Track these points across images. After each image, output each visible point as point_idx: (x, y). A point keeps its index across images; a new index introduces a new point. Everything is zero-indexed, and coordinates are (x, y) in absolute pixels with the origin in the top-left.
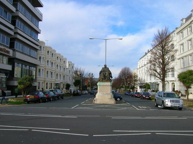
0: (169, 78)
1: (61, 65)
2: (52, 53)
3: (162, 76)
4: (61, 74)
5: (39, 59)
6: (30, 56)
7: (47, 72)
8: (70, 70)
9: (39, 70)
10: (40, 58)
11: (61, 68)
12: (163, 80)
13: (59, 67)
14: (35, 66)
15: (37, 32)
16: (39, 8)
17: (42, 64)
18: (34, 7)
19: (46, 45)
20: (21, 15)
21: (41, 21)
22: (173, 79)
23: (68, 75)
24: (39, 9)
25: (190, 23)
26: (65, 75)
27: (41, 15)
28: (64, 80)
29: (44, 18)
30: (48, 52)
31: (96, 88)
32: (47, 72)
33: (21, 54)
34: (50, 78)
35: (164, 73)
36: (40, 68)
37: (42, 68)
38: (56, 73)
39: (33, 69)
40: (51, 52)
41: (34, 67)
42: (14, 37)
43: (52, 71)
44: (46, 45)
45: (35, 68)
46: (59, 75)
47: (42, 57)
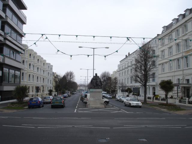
0: (151, 83)
1: (34, 64)
2: (34, 55)
3: (144, 81)
4: (35, 75)
5: (22, 63)
6: (15, 60)
7: (29, 75)
8: (48, 73)
9: (23, 73)
10: (23, 62)
11: (35, 67)
12: (145, 85)
13: (32, 66)
14: (19, 69)
15: (21, 36)
16: (23, 10)
17: (25, 67)
18: (19, 9)
19: (47, 62)
20: (9, 21)
21: (25, 24)
22: (154, 83)
23: (47, 78)
24: (23, 11)
25: (170, 31)
26: (45, 78)
27: (25, 18)
28: (37, 82)
29: (28, 22)
30: (30, 55)
31: (94, 80)
32: (29, 75)
33: (14, 61)
34: (32, 82)
35: (145, 79)
36: (24, 72)
37: (25, 72)
38: (29, 74)
39: (18, 73)
40: (33, 55)
41: (18, 71)
42: (3, 43)
43: (38, 76)
44: (47, 62)
45: (19, 72)
46: (31, 77)
47: (25, 61)
